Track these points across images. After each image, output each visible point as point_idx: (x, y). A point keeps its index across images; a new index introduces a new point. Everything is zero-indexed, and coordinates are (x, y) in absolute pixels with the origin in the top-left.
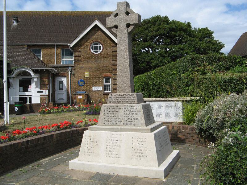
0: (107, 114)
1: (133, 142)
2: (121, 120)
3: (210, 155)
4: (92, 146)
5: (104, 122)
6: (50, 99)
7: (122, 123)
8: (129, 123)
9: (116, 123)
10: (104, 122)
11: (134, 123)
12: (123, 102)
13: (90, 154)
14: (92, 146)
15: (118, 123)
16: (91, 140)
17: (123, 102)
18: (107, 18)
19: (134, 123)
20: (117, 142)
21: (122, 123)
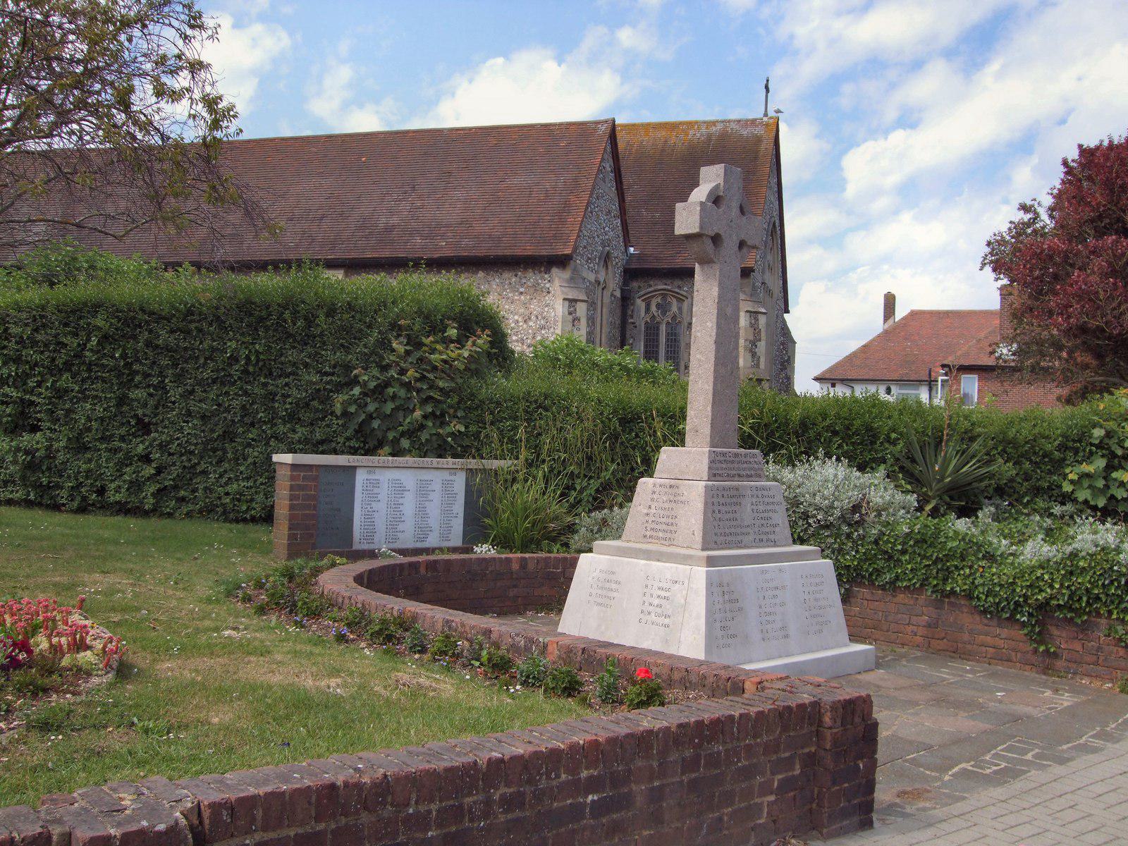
0: (719, 512)
1: (645, 598)
2: (749, 530)
3: (504, 790)
4: (729, 615)
5: (715, 538)
6: (794, 552)
7: (751, 538)
8: (765, 537)
9: (739, 538)
10: (715, 538)
11: (772, 537)
12: (739, 475)
13: (730, 641)
14: (729, 615)
15: (746, 539)
16: (726, 597)
17: (739, 475)
18: (679, 206)
19: (772, 537)
20: (777, 592)
21: (751, 538)
